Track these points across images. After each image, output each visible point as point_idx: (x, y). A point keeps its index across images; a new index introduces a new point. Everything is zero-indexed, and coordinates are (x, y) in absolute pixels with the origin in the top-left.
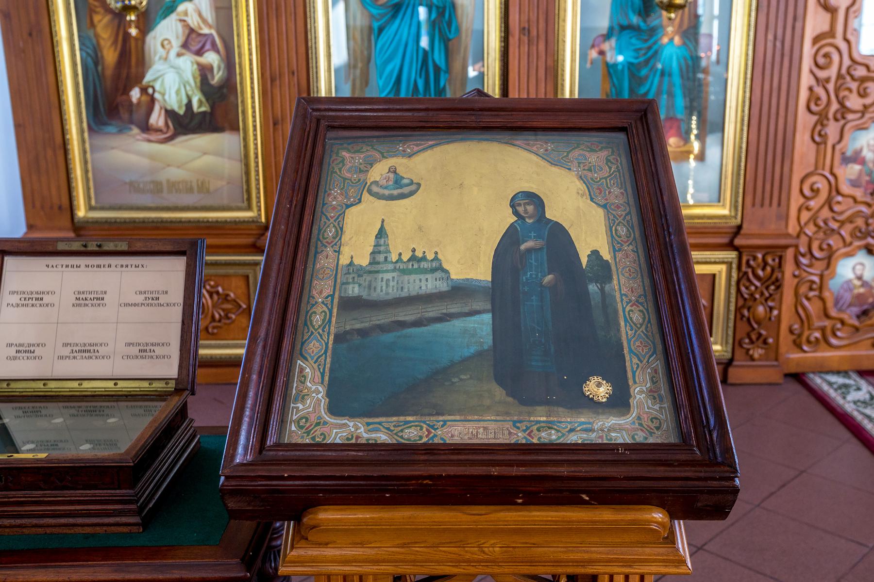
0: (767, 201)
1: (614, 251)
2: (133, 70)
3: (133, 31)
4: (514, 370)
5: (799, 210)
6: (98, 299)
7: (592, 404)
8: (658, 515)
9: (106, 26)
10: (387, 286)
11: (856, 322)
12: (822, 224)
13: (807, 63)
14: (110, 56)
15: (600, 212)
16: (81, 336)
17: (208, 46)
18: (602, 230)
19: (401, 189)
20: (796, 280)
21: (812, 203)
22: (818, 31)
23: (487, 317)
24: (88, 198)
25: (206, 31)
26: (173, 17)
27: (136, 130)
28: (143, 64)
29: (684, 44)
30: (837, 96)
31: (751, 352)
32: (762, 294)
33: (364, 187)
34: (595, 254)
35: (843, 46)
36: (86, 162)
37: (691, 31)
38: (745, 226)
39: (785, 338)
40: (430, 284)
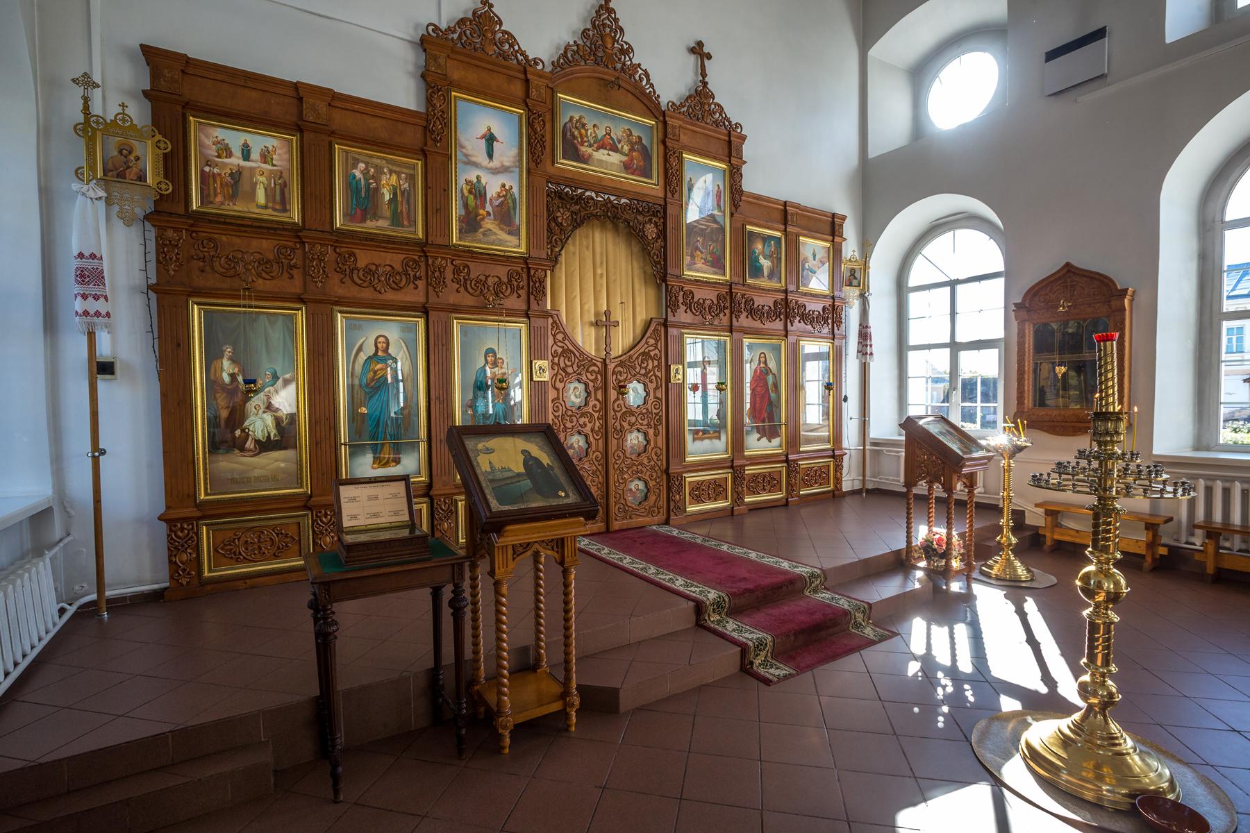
4: (538, 490)
6: (376, 498)
13: (551, 410)
16: (374, 510)
24: (206, 489)
28: (243, 417)
37: (1082, 507)
40: (511, 474)
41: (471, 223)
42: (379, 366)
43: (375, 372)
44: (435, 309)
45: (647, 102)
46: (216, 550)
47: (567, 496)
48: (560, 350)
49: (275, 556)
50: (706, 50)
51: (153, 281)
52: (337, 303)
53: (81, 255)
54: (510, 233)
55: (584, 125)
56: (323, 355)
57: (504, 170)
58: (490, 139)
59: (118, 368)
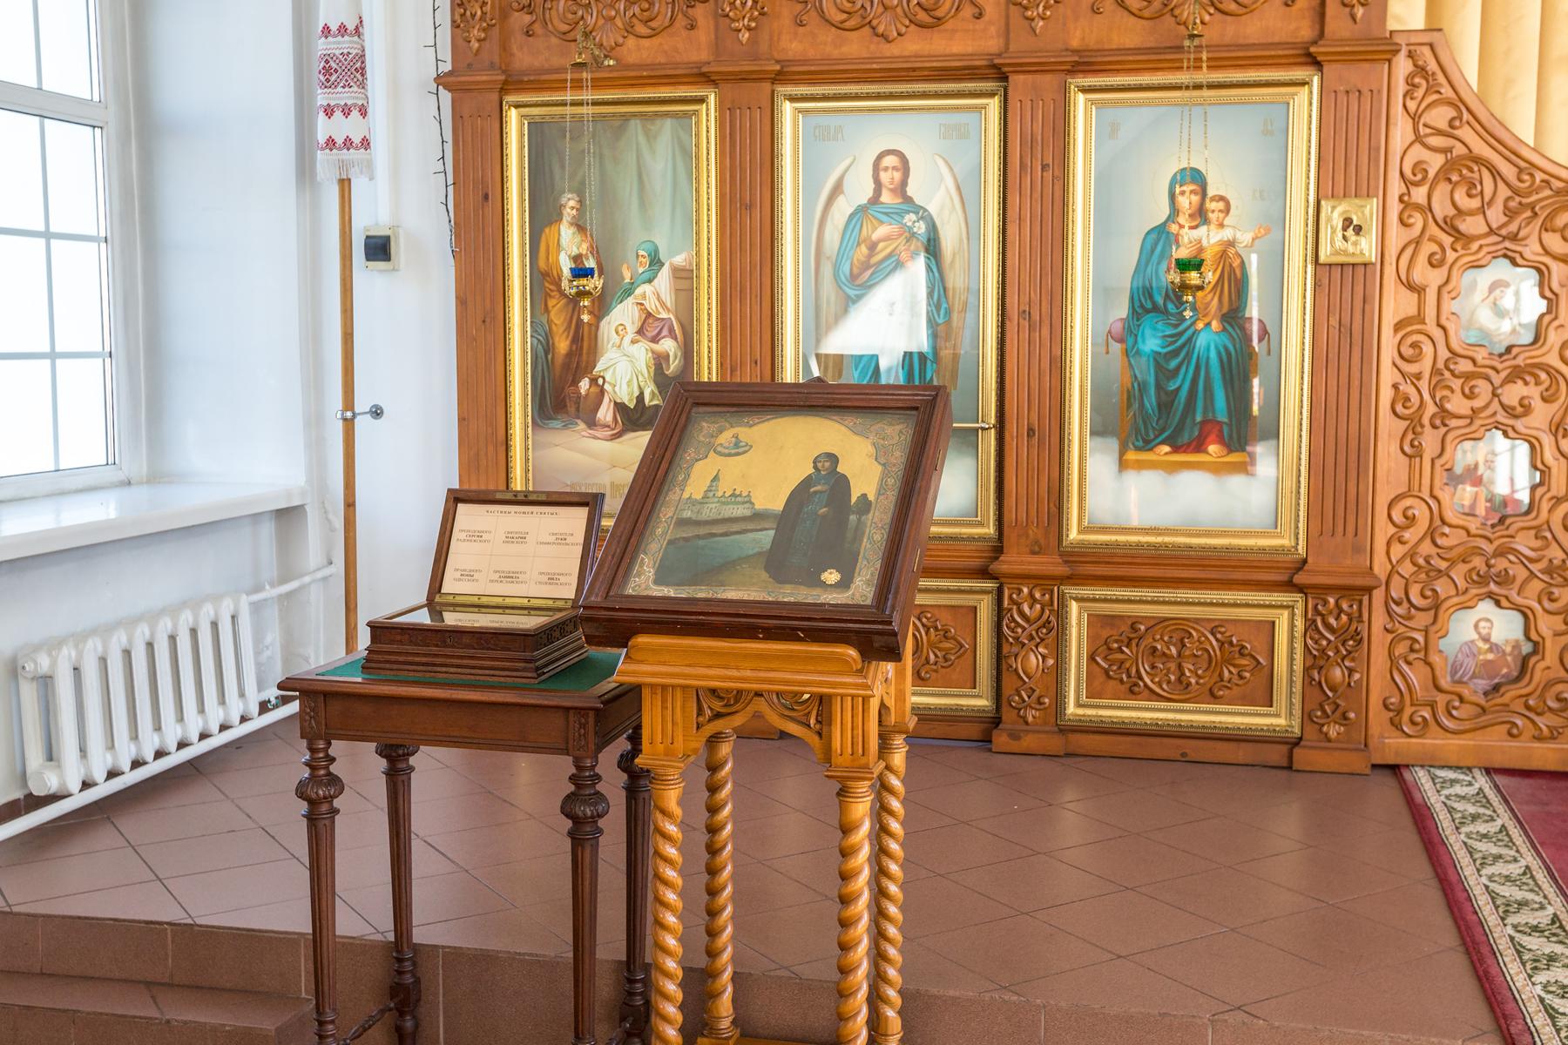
0: (1340, 529)
1: (879, 494)
2: (584, 357)
3: (586, 318)
5: (1389, 544)
6: (521, 538)
7: (823, 585)
8: (852, 652)
9: (561, 311)
10: (710, 511)
11: (1482, 701)
12: (1421, 561)
14: (562, 345)
15: (880, 468)
17: (665, 332)
18: (876, 480)
19: (739, 449)
20: (1390, 637)
21: (1407, 535)
22: (1402, 316)
23: (772, 533)
25: (664, 315)
26: (630, 300)
27: (582, 426)
29: (1224, 329)
30: (1433, 397)
31: (1325, 729)
32: (1338, 651)
33: (710, 447)
34: (864, 495)
35: (1437, 334)
36: (527, 460)
38: (1310, 560)
39: (1378, 718)
40: (740, 511)
42: (882, 231)
43: (872, 247)
44: (1022, 68)
46: (1092, 658)
47: (844, 584)
48: (1436, 162)
49: (1213, 697)
51: (446, 67)
52: (781, 77)
53: (326, 31)
56: (751, 206)
59: (399, 249)
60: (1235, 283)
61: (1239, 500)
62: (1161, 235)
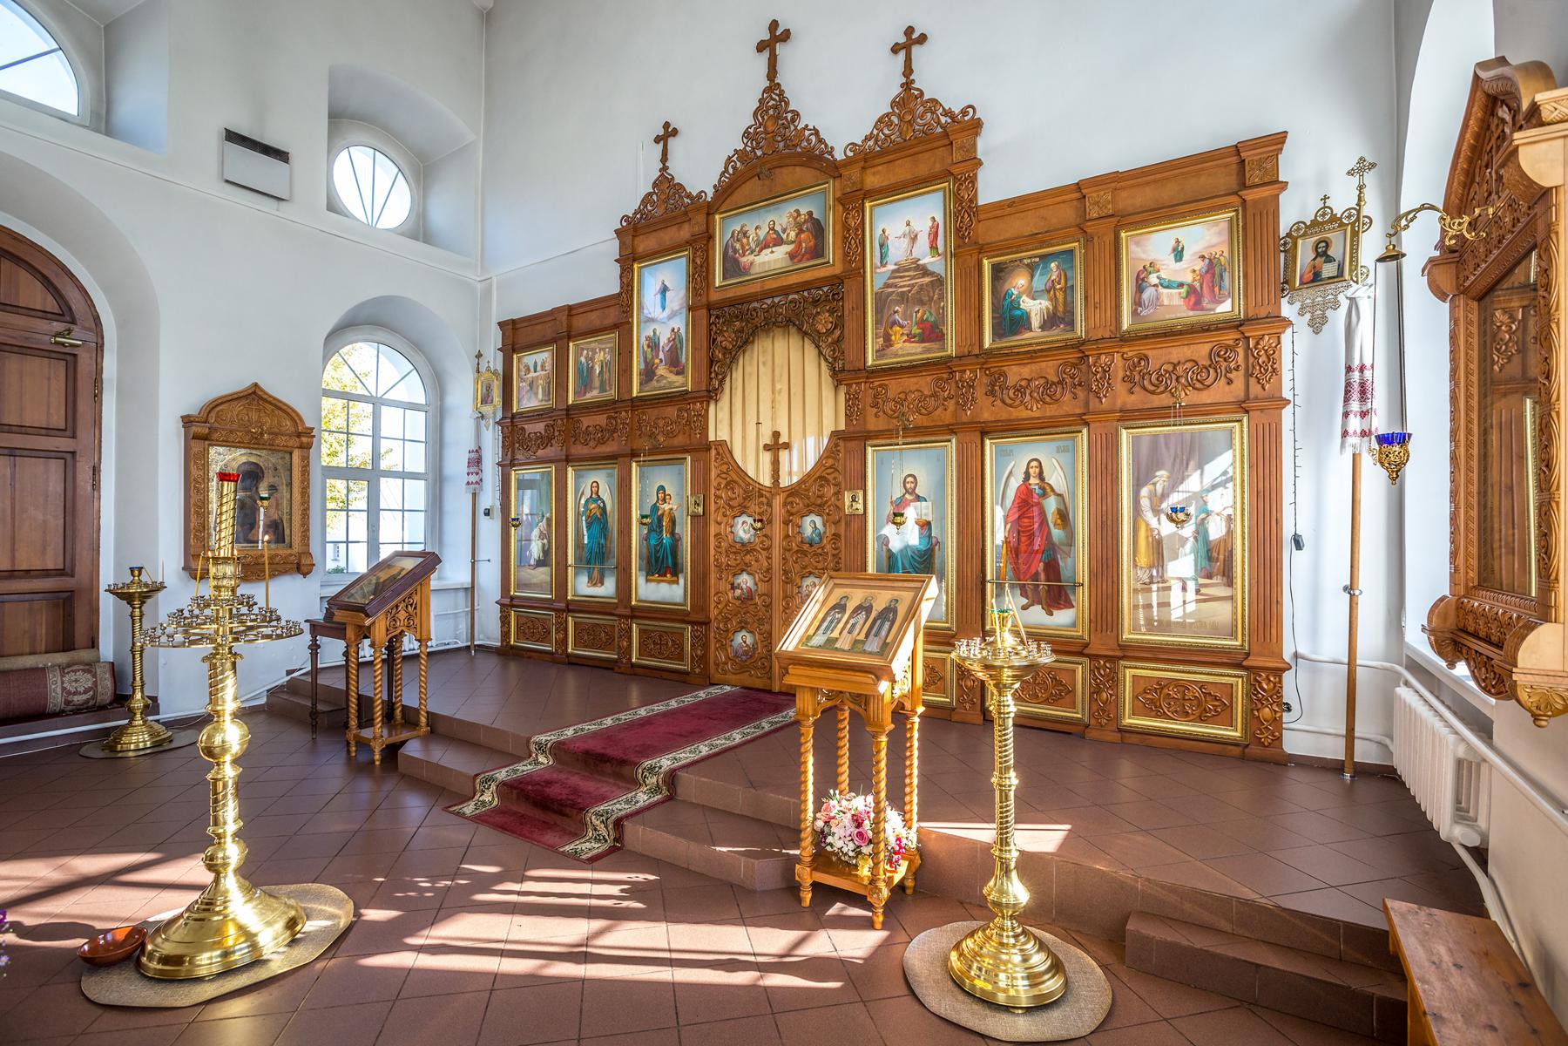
41: (649, 374)
45: (813, 159)
49: (1046, 701)
50: (661, 132)
54: (678, 373)
55: (745, 234)
57: (673, 315)
58: (664, 290)
60: (673, 522)
61: (671, 592)
62: (655, 508)
